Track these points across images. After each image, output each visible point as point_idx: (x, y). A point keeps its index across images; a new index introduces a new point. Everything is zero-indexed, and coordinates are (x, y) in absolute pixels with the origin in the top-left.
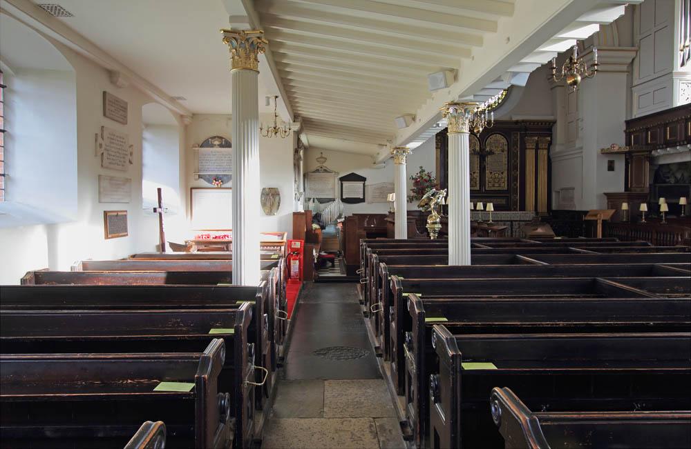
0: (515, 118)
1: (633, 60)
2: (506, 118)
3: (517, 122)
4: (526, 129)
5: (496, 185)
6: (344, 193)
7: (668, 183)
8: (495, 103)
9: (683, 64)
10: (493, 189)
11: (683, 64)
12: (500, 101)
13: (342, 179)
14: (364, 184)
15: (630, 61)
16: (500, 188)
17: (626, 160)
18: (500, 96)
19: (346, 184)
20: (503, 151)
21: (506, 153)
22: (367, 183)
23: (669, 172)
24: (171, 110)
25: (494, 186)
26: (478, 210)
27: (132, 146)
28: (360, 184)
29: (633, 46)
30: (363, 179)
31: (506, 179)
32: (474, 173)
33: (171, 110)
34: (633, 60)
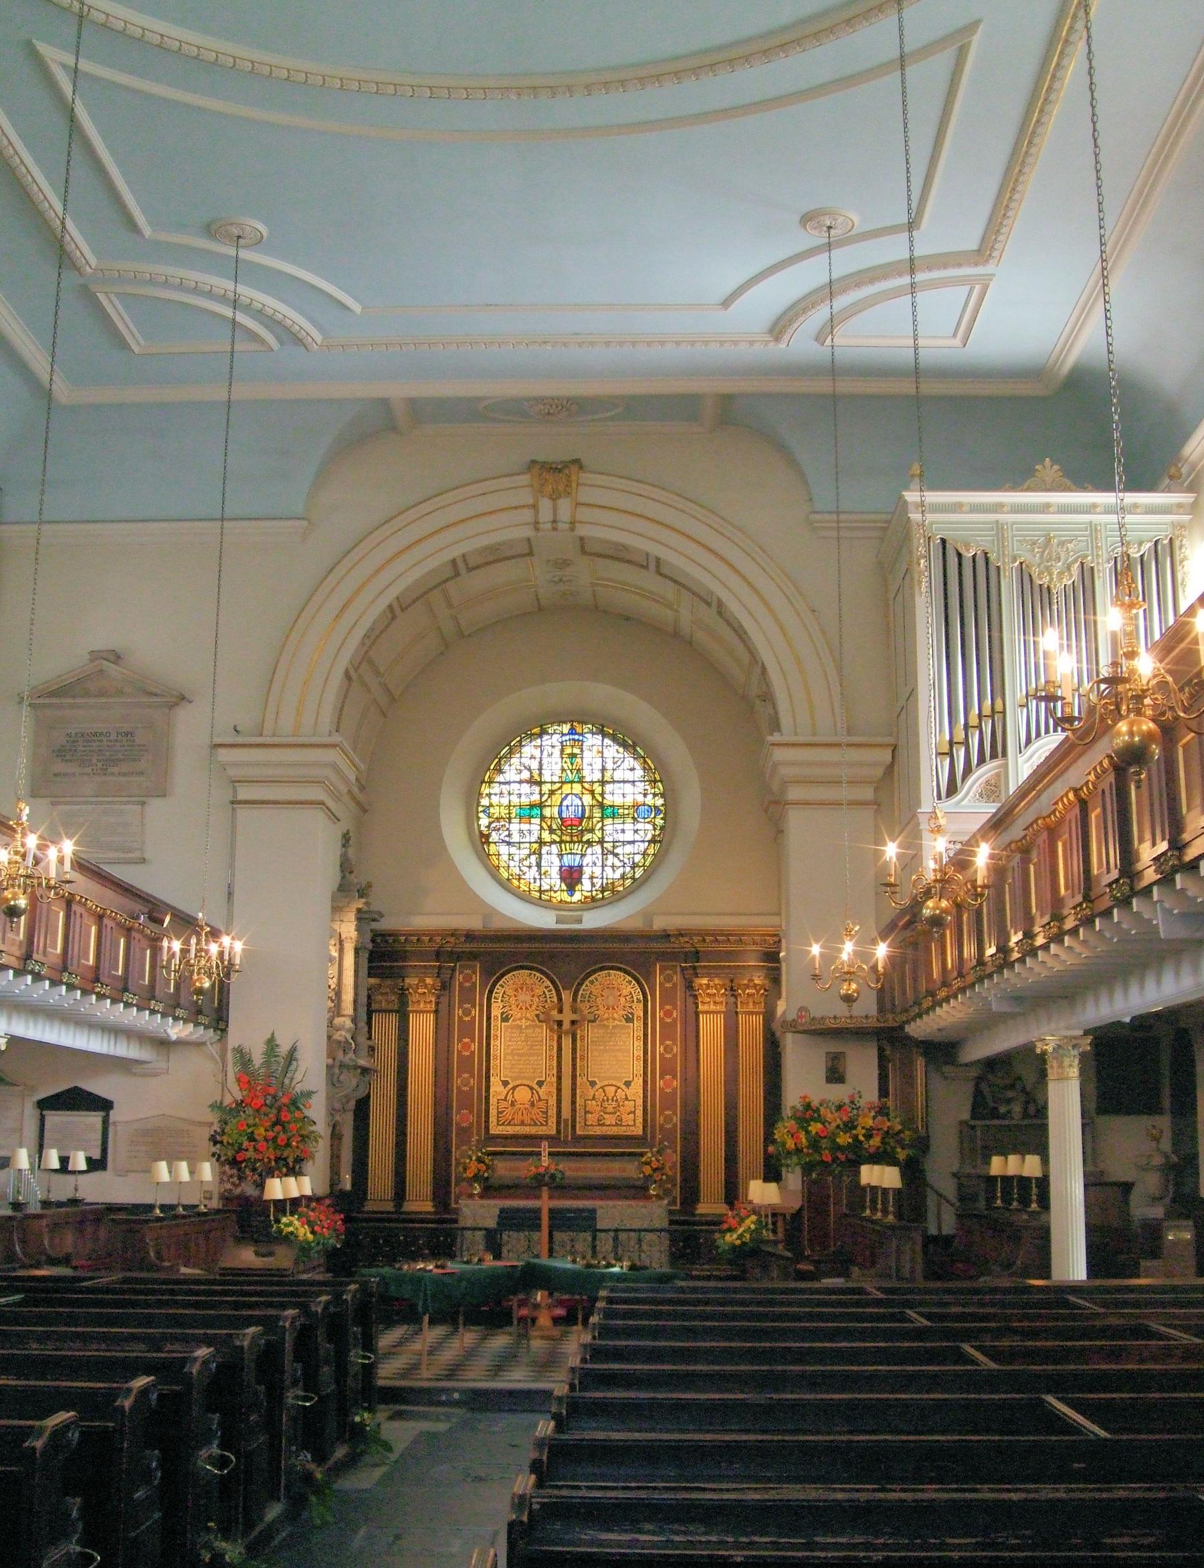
0: (659, 924)
2: (638, 924)
3: (666, 936)
4: (697, 955)
5: (610, 1119)
6: (99, 1136)
7: (1004, 1117)
8: (623, 877)
9: (952, 790)
10: (598, 1131)
12: (639, 873)
13: (45, 1105)
14: (105, 1122)
15: (879, 772)
16: (620, 1131)
17: (881, 1050)
18: (638, 858)
19: (54, 1119)
20: (629, 1020)
21: (638, 1024)
22: (114, 1115)
23: (1012, 1086)
24: (612, 418)
25: (601, 1124)
26: (73, 1172)
27: (235, 727)
28: (94, 1119)
29: (891, 735)
30: (104, 1105)
31: (640, 1102)
32: (540, 1084)
33: (612, 418)
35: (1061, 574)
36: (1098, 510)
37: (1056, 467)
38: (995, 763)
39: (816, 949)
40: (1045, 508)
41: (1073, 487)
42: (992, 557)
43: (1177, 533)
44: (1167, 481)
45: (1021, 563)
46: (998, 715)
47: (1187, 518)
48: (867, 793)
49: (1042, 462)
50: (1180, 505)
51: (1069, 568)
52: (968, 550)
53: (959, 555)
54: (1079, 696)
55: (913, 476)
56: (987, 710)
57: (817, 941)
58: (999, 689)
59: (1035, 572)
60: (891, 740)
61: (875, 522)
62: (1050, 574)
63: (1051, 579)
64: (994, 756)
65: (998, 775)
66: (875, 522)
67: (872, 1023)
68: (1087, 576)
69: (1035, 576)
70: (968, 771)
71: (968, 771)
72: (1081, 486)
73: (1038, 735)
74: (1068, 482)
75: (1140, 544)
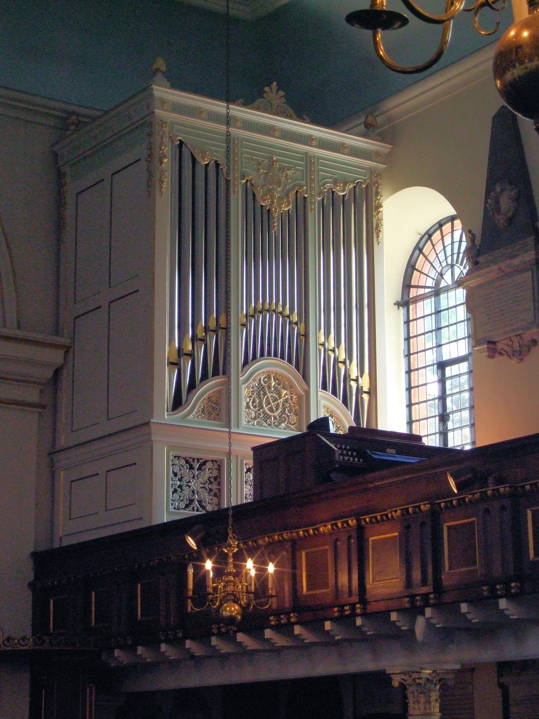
1: (57, 372)
11: (177, 403)
15: (49, 374)
34: (57, 372)
35: (281, 198)
36: (314, 143)
37: (281, 93)
38: (212, 383)
39: (271, 568)
40: (270, 130)
41: (294, 116)
42: (223, 167)
43: (374, 179)
44: (362, 127)
45: (247, 181)
46: (223, 330)
47: (382, 166)
48: (32, 395)
49: (269, 85)
50: (377, 154)
51: (287, 195)
52: (203, 158)
53: (194, 161)
54: (291, 323)
55: (157, 70)
56: (212, 324)
57: (210, 556)
58: (225, 306)
59: (259, 193)
60: (64, 341)
61: (54, 109)
62: (273, 197)
63: (273, 202)
64: (216, 373)
65: (219, 392)
66: (54, 109)
67: (29, 645)
68: (301, 206)
69: (258, 196)
70: (192, 386)
71: (192, 386)
72: (300, 116)
73: (254, 357)
74: (291, 112)
75: (345, 184)
